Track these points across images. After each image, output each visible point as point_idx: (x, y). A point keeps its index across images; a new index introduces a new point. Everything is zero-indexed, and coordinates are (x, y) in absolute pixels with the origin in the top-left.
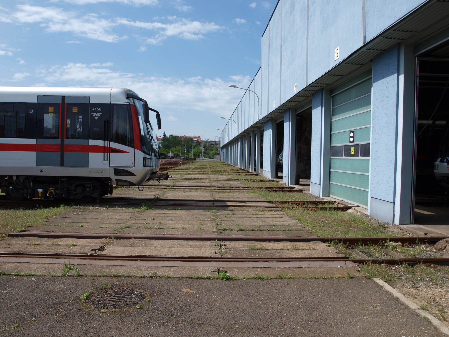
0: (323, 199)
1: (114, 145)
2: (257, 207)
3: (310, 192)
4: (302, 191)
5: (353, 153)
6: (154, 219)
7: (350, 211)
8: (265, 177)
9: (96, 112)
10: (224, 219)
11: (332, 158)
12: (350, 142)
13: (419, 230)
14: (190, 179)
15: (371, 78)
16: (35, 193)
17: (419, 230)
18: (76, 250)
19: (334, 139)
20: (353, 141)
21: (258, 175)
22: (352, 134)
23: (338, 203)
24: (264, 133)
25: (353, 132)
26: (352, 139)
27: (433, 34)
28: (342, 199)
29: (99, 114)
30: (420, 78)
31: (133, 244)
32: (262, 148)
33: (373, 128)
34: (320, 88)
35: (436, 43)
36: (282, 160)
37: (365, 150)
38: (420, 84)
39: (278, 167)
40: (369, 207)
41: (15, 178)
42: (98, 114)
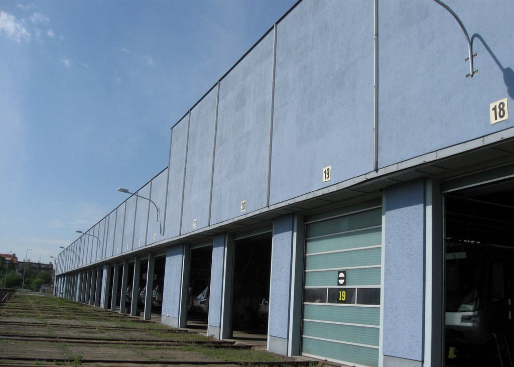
0: (293, 358)
4: (250, 347)
5: (344, 299)
8: (169, 326)
11: (305, 303)
12: (339, 284)
15: (381, 208)
19: (309, 279)
20: (344, 284)
21: (147, 322)
22: (342, 275)
24: (167, 259)
25: (344, 272)
26: (341, 282)
27: (465, 175)
28: (324, 359)
35: (488, 180)
36: (207, 302)
39: (195, 314)
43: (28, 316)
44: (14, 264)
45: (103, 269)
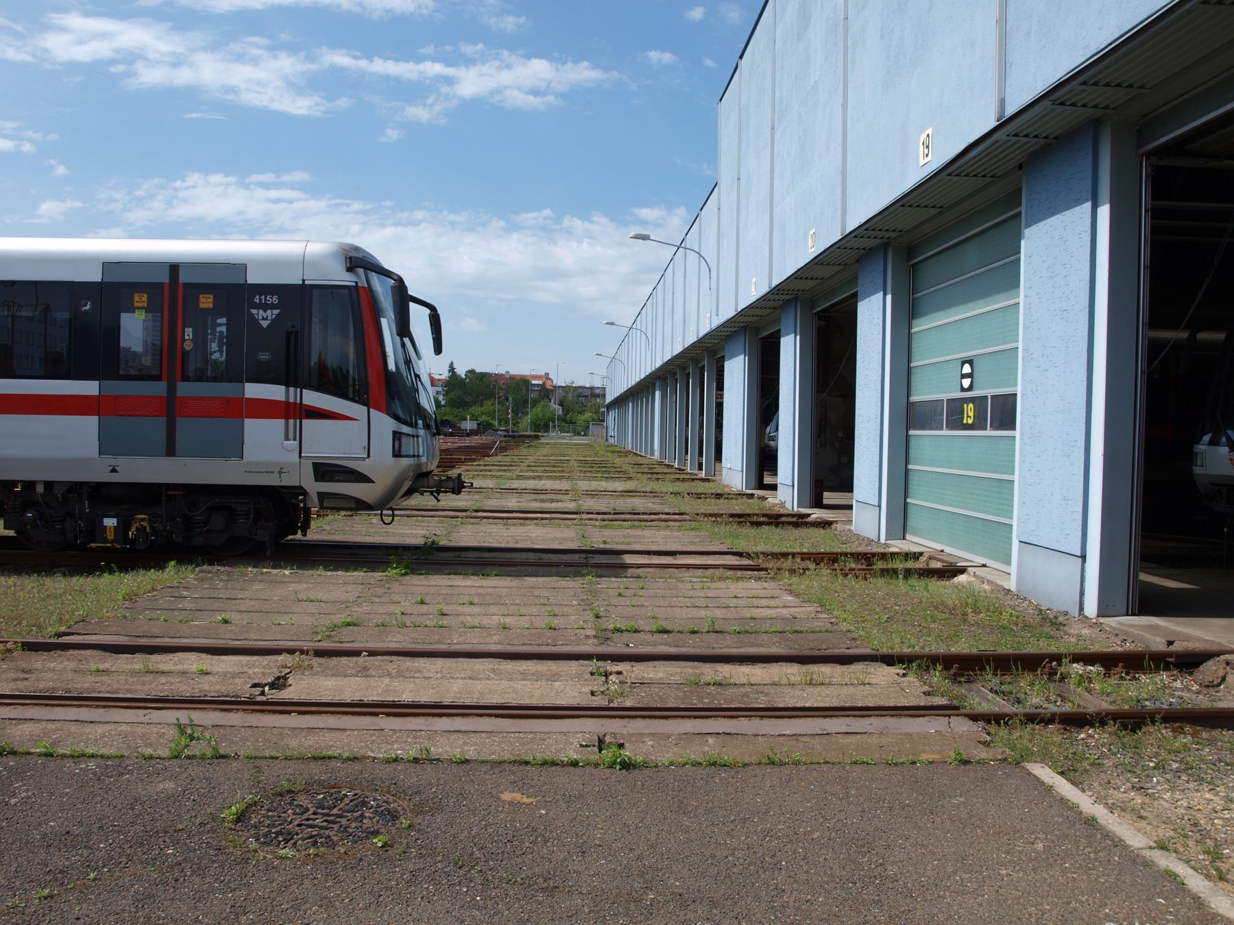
0: (887, 546)
1: (313, 398)
2: (705, 567)
3: (853, 528)
4: (830, 523)
5: (970, 421)
6: (422, 602)
7: (962, 578)
8: (727, 486)
9: (265, 307)
10: (615, 601)
11: (911, 432)
12: (963, 390)
13: (1152, 632)
14: (523, 492)
15: (1019, 214)
16: (95, 529)
17: (1152, 632)
18: (208, 687)
19: (918, 381)
20: (970, 388)
21: (708, 480)
22: (967, 369)
23: (930, 558)
24: (727, 364)
25: (970, 362)
26: (966, 383)
27: (1190, 94)
28: (939, 547)
29: (272, 314)
30: (1155, 213)
31: (366, 668)
32: (720, 406)
33: (1024, 350)
34: (879, 241)
35: (1199, 118)
36: (775, 439)
37: (1003, 413)
38: (1154, 230)
39: (764, 459)
40: (1013, 569)
41: (40, 489)
42: (269, 312)
43: (550, 478)
44: (547, 390)
45: (853, 300)
